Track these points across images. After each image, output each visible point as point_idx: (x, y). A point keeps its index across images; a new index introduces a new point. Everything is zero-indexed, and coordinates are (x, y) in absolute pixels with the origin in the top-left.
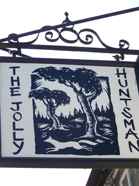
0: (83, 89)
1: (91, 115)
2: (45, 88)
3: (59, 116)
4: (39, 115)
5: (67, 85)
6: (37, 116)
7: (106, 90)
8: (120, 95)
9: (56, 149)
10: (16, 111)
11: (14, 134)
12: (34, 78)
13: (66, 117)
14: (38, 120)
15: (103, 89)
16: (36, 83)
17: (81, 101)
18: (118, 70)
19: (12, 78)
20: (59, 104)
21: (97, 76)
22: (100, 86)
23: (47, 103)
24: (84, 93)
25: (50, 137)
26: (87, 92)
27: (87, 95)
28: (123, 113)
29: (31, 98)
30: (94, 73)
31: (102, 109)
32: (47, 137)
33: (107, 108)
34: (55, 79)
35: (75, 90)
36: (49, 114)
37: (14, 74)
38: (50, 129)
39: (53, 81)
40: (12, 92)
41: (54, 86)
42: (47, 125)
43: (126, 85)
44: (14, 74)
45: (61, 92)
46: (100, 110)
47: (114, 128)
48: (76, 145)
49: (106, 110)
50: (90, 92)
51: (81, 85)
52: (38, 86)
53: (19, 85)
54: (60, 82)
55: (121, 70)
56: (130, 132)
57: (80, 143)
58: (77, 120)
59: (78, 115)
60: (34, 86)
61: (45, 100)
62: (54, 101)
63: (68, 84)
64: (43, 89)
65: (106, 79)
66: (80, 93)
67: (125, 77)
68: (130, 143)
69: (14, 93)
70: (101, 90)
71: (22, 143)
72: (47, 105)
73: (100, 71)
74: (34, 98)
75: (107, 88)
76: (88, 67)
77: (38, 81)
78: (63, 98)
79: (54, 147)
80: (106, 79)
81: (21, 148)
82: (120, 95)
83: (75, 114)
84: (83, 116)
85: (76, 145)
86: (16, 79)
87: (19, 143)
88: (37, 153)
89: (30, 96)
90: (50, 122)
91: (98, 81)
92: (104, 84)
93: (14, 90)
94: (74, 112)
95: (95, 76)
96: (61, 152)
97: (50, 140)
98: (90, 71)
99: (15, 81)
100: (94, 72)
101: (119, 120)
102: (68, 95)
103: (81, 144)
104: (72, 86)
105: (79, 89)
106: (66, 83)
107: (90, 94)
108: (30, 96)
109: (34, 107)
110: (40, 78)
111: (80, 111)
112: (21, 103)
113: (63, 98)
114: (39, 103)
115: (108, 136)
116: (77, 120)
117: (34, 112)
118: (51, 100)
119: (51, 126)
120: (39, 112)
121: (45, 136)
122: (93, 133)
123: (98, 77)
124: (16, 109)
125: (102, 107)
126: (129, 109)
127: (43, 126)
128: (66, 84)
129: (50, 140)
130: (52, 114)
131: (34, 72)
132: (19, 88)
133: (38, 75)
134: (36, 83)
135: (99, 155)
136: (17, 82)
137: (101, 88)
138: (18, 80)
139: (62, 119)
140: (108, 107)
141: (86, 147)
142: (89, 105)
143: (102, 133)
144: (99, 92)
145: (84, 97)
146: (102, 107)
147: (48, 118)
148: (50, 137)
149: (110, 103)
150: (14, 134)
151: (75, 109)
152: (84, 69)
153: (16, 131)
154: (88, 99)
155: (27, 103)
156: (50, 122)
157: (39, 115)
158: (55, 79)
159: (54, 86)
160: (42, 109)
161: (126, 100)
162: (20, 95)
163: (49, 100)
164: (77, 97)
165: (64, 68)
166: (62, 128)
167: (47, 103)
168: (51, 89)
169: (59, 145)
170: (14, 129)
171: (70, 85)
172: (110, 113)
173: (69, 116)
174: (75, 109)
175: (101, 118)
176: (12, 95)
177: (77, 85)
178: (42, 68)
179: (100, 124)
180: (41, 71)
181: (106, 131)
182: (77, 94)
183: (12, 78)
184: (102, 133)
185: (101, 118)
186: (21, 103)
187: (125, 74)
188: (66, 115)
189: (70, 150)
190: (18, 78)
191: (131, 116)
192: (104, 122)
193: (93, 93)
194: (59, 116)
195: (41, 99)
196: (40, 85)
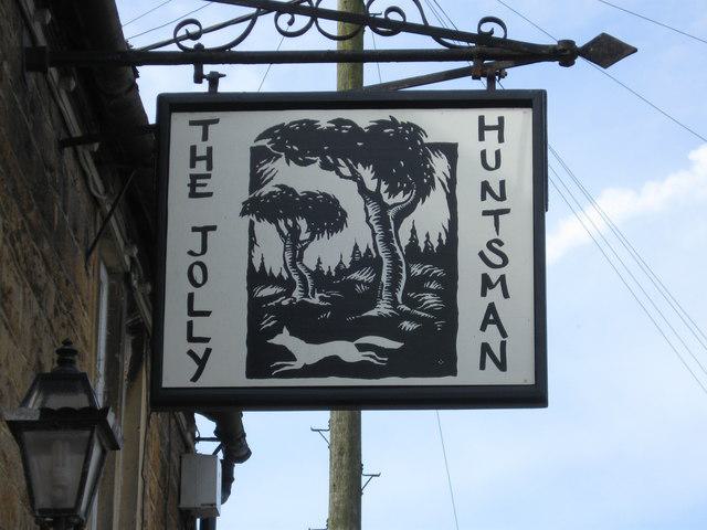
0: (384, 187)
1: (394, 258)
2: (283, 187)
3: (314, 269)
4: (262, 265)
5: (342, 176)
6: (258, 270)
7: (444, 187)
8: (483, 198)
9: (297, 365)
10: (198, 255)
11: (190, 325)
12: (258, 155)
13: (329, 272)
14: (257, 277)
15: (437, 183)
16: (263, 171)
17: (373, 223)
18: (481, 119)
19: (193, 149)
20: (315, 232)
21: (425, 140)
22: (431, 171)
23: (286, 232)
24: (385, 197)
25: (285, 329)
26: (393, 192)
27: (390, 202)
28: (482, 254)
29: (247, 219)
30: (416, 131)
31: (426, 242)
32: (276, 330)
33: (440, 240)
34: (314, 158)
35: (362, 190)
36: (288, 261)
37: (205, 138)
38: (285, 303)
39: (306, 163)
40: (193, 185)
41: (309, 178)
42: (280, 290)
43: (498, 165)
44: (205, 138)
45: (325, 195)
46: (422, 245)
47: (449, 313)
48: (347, 351)
49: (436, 244)
50: (402, 193)
51: (379, 175)
52: (266, 183)
53: (210, 167)
54: (325, 166)
55: (491, 116)
56: (491, 317)
57: (357, 345)
58: (356, 276)
59: (364, 260)
60: (256, 181)
61: (282, 224)
62: (303, 224)
63: (345, 171)
64: (277, 189)
65: (450, 151)
66: (375, 197)
67: (501, 139)
68: (486, 348)
69: (199, 190)
70: (432, 183)
71: (208, 351)
72: (286, 238)
73: (437, 125)
74: (254, 219)
75: (449, 176)
76: (403, 116)
77: (269, 166)
78: (326, 215)
79: (296, 360)
80: (450, 151)
81: (202, 363)
82: (483, 198)
83: (353, 262)
84: (376, 264)
85: (347, 351)
86: (204, 153)
87: (199, 349)
88: (250, 375)
89: (243, 213)
90: (289, 286)
91: (426, 158)
92: (440, 164)
93: (198, 181)
94: (353, 256)
95: (421, 141)
96: (308, 371)
97: (284, 339)
98: (409, 125)
99: (201, 159)
100: (418, 129)
101: (469, 270)
102: (343, 205)
103: (362, 348)
104: (355, 177)
105: (371, 185)
106: (341, 169)
107: (400, 198)
108: (243, 213)
109: (252, 243)
110: (274, 155)
111: (368, 250)
112: (214, 228)
113: (326, 215)
114: (265, 230)
115: (430, 311)
116: (356, 276)
117: (251, 257)
118: (295, 223)
119: (288, 294)
120: (262, 259)
121: (270, 325)
122: (394, 303)
123: (429, 145)
124: (198, 251)
125: (427, 235)
126: (501, 244)
127: (269, 291)
128: (338, 173)
129: (284, 339)
130: (293, 265)
131: (261, 137)
132: (209, 176)
133: (269, 147)
134: (263, 171)
135: (404, 375)
136: (205, 162)
137: (432, 177)
138: (209, 158)
139: (320, 279)
140: (444, 238)
141: (374, 354)
142: (392, 230)
143: (413, 303)
144: (423, 192)
145: (384, 208)
146: (427, 235)
147: (285, 275)
148: (285, 329)
149: (453, 222)
150: (190, 325)
151: (356, 247)
152: (393, 123)
153: (196, 320)
154: (391, 213)
155: (232, 227)
156: (289, 286)
157: (262, 265)
158: (314, 158)
159: (309, 178)
160: (272, 253)
161: (496, 214)
162: (210, 194)
163: (290, 222)
164: (366, 209)
165: (339, 122)
166: (315, 301)
167: (286, 232)
168: (300, 189)
169: (307, 353)
170: (192, 313)
171: (349, 174)
172: (446, 255)
173: (337, 269)
174: (356, 247)
175: (417, 270)
176: (193, 195)
177: (367, 174)
178: (281, 127)
179: (416, 284)
180: (278, 134)
181: (424, 300)
182: (366, 202)
183: (193, 149)
184: (413, 303)
185: (417, 270)
186: (214, 228)
187: (500, 127)
188: (329, 264)
189: (332, 365)
190: (210, 150)
191: (505, 261)
192: (425, 278)
193: (407, 196)
194: (314, 269)
195: (273, 220)
196: (272, 178)
